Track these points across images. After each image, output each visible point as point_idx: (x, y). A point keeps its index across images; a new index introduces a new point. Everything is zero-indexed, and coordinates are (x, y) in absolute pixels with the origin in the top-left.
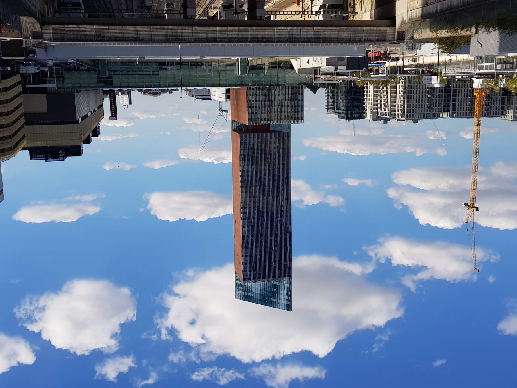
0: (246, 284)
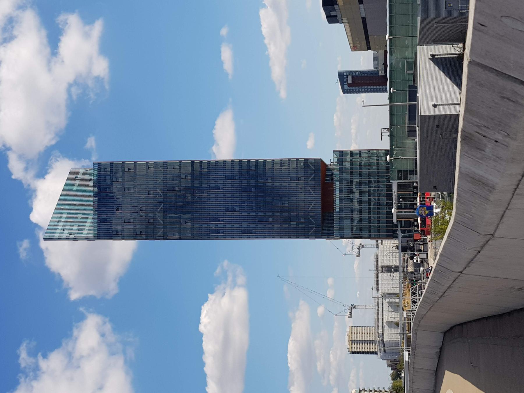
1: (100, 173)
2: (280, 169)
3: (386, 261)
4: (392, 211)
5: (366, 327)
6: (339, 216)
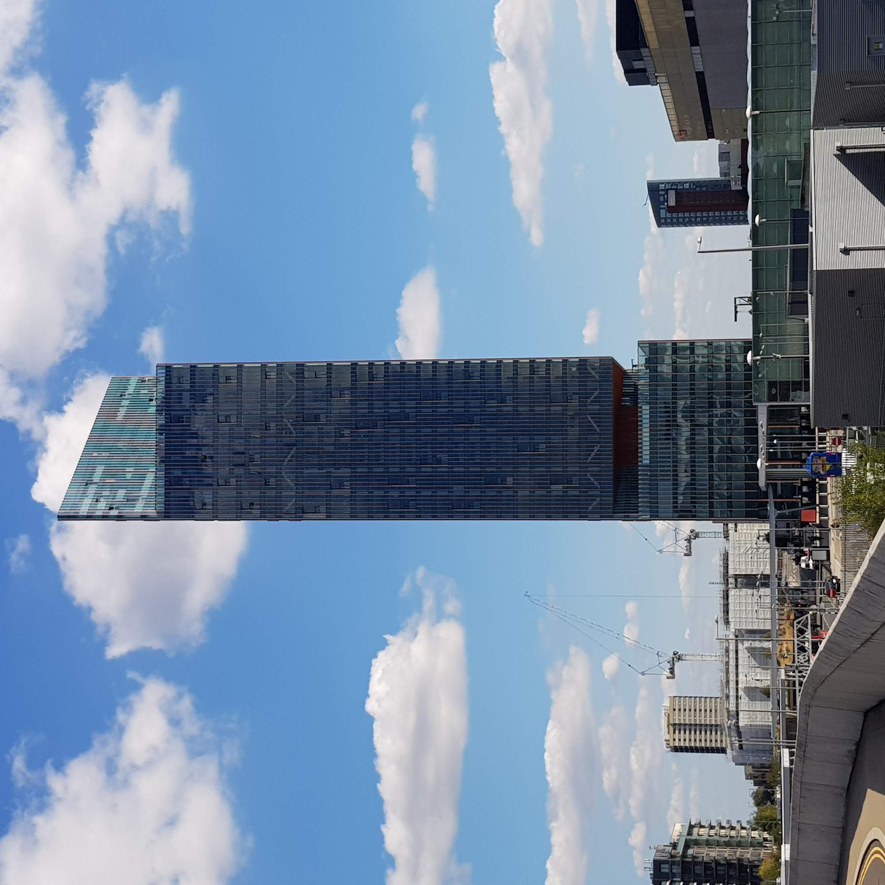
0: (154, 402)
1: (169, 387)
4: (756, 465)
6: (649, 474)
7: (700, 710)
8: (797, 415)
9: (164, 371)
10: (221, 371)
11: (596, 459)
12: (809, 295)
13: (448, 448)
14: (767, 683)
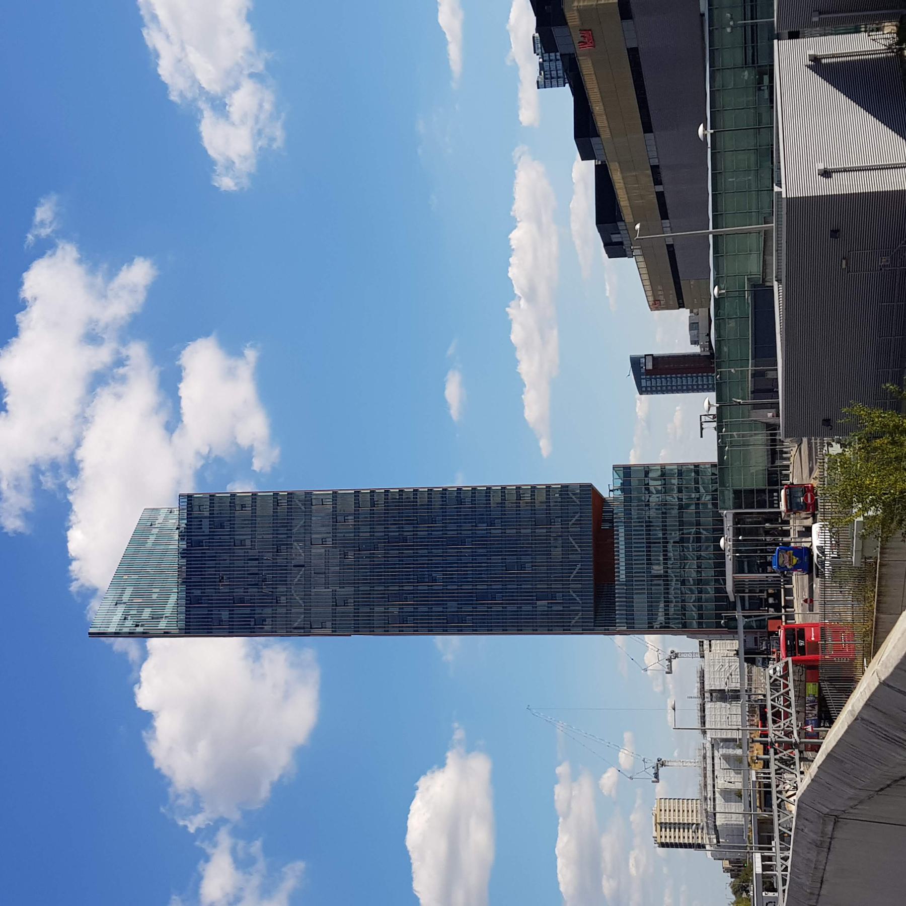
1: (191, 514)
2: (516, 503)
3: (718, 681)
4: (719, 545)
5: (685, 801)
6: (625, 588)
7: (683, 811)
8: (762, 532)
9: (186, 500)
10: (237, 499)
11: (572, 569)
12: (775, 284)
13: (442, 567)
14: (739, 786)
